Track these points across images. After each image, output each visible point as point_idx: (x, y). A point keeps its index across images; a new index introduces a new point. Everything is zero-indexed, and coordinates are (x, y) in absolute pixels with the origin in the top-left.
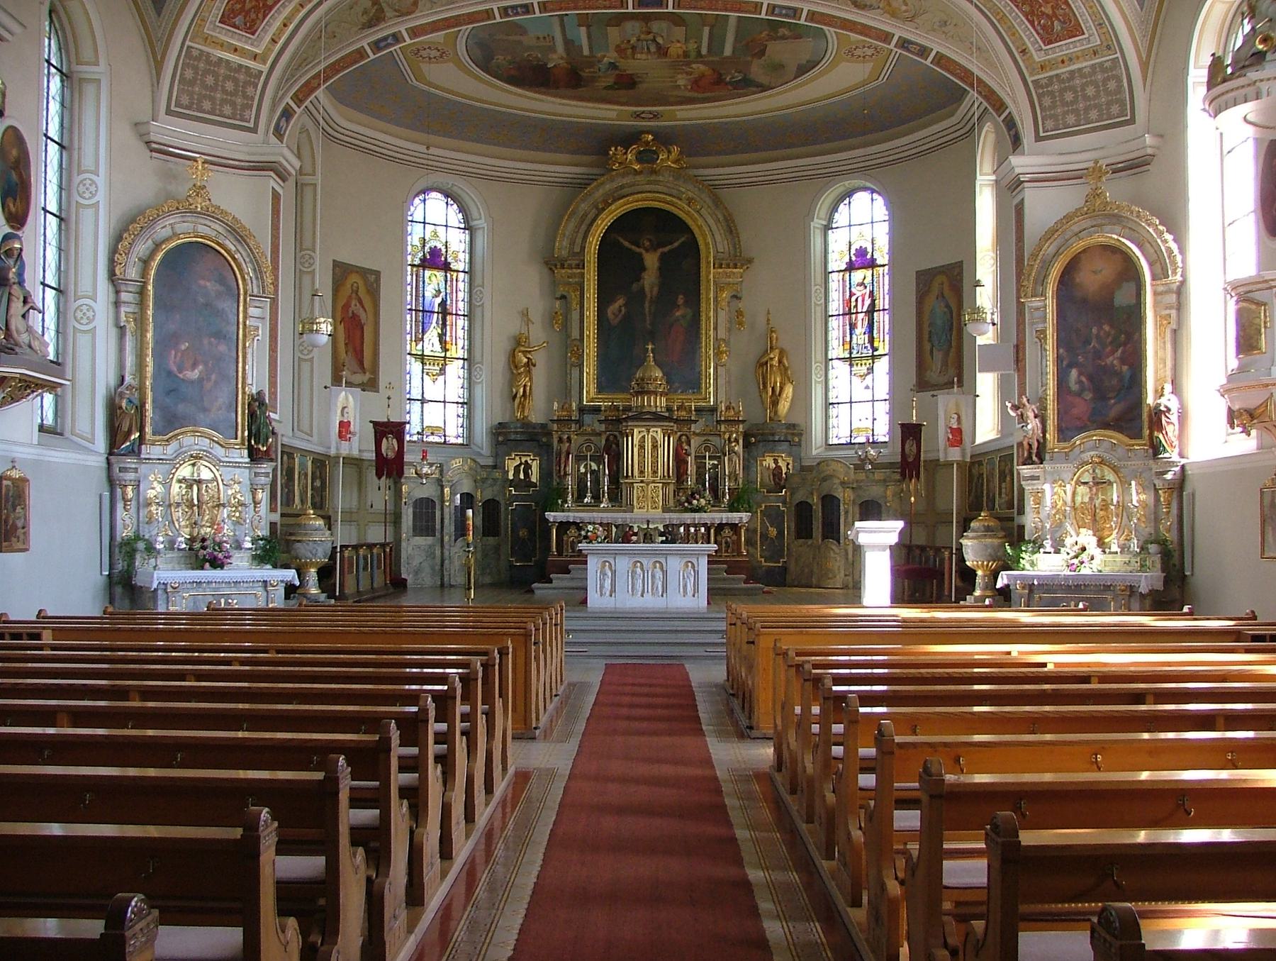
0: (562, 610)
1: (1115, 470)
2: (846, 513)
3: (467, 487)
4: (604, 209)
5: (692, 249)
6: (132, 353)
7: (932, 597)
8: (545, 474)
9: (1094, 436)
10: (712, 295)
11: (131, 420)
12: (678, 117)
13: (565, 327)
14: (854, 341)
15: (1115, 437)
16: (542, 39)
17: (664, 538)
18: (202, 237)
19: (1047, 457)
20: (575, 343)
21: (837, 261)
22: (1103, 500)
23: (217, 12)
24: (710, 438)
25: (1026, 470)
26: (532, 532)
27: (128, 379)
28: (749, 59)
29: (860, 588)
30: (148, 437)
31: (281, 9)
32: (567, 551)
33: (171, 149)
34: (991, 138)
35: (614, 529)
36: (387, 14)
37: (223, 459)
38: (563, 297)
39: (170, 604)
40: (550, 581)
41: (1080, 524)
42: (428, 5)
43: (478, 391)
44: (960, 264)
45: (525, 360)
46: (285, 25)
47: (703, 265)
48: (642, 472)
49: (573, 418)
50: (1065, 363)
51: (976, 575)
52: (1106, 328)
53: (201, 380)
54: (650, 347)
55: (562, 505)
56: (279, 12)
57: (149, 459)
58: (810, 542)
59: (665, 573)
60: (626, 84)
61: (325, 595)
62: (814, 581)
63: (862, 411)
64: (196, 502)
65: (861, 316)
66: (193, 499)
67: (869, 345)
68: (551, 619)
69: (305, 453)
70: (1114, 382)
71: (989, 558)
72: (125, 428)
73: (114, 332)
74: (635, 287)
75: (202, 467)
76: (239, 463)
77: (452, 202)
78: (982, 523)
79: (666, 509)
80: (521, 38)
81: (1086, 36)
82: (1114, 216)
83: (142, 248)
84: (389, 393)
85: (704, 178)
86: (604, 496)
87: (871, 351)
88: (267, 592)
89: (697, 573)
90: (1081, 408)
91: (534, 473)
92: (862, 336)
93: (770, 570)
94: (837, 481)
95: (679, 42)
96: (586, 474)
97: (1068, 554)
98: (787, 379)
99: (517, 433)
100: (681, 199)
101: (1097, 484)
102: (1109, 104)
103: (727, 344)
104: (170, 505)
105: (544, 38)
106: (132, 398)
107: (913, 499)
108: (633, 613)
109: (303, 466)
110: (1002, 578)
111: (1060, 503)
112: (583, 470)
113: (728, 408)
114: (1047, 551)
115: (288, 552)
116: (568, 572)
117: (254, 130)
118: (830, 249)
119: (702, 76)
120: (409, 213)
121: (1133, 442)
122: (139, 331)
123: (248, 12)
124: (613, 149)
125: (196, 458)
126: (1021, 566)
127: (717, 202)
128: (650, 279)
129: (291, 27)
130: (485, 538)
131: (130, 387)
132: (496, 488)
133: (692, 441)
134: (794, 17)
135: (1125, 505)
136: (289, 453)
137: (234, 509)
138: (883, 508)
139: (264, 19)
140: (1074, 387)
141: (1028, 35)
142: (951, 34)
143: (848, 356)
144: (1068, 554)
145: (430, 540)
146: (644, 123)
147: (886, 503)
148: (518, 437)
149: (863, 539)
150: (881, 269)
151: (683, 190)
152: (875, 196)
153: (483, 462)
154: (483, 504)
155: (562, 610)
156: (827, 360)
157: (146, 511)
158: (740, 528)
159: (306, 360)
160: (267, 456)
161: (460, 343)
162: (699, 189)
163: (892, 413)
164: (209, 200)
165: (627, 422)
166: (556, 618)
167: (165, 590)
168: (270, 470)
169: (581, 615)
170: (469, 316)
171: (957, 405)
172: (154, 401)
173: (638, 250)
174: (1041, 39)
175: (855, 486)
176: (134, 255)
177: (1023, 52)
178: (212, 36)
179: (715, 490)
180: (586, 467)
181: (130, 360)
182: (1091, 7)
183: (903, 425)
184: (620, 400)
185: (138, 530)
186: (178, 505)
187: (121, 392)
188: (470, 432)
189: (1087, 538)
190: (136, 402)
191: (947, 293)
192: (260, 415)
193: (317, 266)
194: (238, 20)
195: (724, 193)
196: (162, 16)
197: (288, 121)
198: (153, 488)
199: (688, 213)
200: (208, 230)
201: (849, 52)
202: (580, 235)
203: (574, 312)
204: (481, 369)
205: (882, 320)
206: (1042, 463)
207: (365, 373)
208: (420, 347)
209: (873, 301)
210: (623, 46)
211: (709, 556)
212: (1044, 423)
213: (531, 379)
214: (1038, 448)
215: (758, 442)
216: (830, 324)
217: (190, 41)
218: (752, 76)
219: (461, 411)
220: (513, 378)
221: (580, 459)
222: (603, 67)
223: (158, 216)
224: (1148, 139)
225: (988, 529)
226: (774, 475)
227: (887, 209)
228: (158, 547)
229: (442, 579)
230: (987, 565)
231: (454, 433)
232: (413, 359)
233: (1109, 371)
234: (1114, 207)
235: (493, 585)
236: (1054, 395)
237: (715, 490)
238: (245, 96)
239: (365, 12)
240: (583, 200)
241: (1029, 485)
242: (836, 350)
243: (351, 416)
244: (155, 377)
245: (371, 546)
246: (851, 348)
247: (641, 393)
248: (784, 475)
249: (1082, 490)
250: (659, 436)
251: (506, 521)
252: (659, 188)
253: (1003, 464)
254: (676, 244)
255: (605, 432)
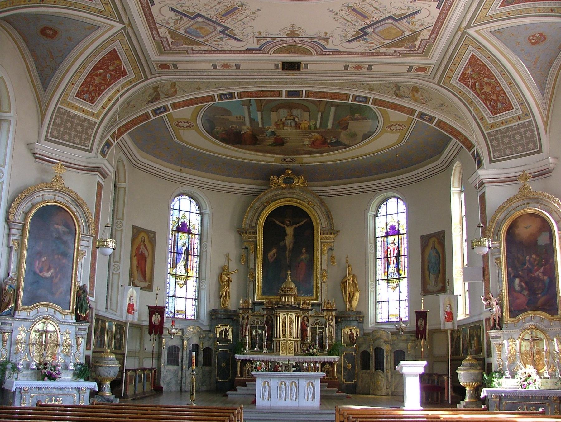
0: (242, 410)
1: (544, 332)
2: (387, 356)
3: (195, 341)
4: (267, 206)
5: (310, 226)
6: (16, 260)
7: (438, 401)
8: (235, 335)
9: (530, 314)
10: (319, 248)
11: (10, 297)
12: (304, 161)
13: (247, 262)
14: (390, 271)
15: (543, 315)
16: (239, 118)
17: (295, 369)
18: (58, 203)
19: (504, 326)
20: (251, 270)
21: (381, 232)
22: (537, 349)
23: (74, 91)
24: (318, 318)
25: (492, 333)
26: (228, 364)
27: (11, 274)
28: (340, 130)
29: (403, 396)
30: (19, 306)
31: (108, 92)
32: (245, 374)
33: (45, 158)
34: (458, 170)
35: (270, 364)
36: (161, 96)
37: (60, 320)
38: (246, 248)
39: (22, 400)
40: (236, 390)
41: (525, 362)
42: (182, 92)
43: (204, 294)
44: (443, 232)
45: (227, 278)
46: (109, 100)
47: (315, 233)
48: (284, 335)
49: (250, 307)
50: (512, 276)
51: (466, 390)
52: (534, 256)
53: (52, 277)
54: (289, 272)
55: (243, 351)
56: (107, 93)
57: (19, 318)
58: (368, 371)
59: (297, 388)
60: (280, 142)
61: (113, 396)
62: (371, 391)
63: (393, 306)
64: (44, 343)
65: (393, 259)
66: (42, 341)
67: (396, 273)
68: (235, 417)
69: (111, 320)
70: (540, 285)
71: (473, 381)
72: (7, 301)
73: (6, 249)
74: (282, 244)
75: (49, 324)
76: (70, 323)
77: (193, 201)
78: (468, 362)
79: (296, 354)
80: (229, 117)
81: (515, 110)
82: (535, 198)
83: (25, 206)
84: (157, 292)
85: (317, 192)
86: (264, 347)
87: (398, 276)
88: (80, 394)
89: (314, 388)
90: (522, 299)
91: (230, 335)
92: (394, 268)
93: (347, 386)
94: (382, 340)
95: (306, 121)
96: (256, 335)
97: (521, 379)
98: (356, 289)
99: (222, 314)
100: (304, 202)
101: (534, 340)
102: (528, 143)
103: (327, 271)
104: (29, 344)
105: (240, 117)
106: (12, 285)
107: (422, 349)
108: (280, 410)
109: (110, 327)
110: (484, 392)
111: (513, 351)
112: (254, 333)
113: (328, 303)
114: (507, 377)
115: (95, 372)
116: (246, 386)
117: (90, 151)
118: (378, 225)
119: (317, 139)
120: (172, 205)
121: (553, 317)
122: (19, 250)
123: (91, 92)
124: (272, 177)
125: (46, 319)
126: (493, 385)
127: (322, 203)
128: (289, 240)
129: (113, 101)
130: (204, 367)
131: (12, 279)
132: (210, 342)
133: (310, 320)
134: (365, 102)
135: (551, 351)
136: (100, 319)
137: (65, 348)
138: (406, 354)
139: (99, 96)
140: (517, 288)
141: (485, 111)
142: (445, 110)
143: (387, 278)
144: (521, 379)
145: (176, 367)
146: (287, 164)
147: (407, 351)
148: (222, 316)
149: (405, 371)
150: (403, 235)
151: (305, 197)
152: (399, 200)
153: (204, 328)
154: (204, 350)
155: (242, 410)
156: (376, 280)
157: (15, 347)
158: (334, 364)
159: (116, 274)
160: (85, 320)
161: (195, 269)
162: (313, 197)
163: (409, 307)
164: (63, 184)
165: (277, 309)
166: (238, 416)
167: (20, 392)
168: (87, 327)
169: (252, 410)
170: (200, 256)
171: (450, 301)
172: (25, 287)
173: (282, 225)
174: (491, 112)
175: (391, 343)
176: (20, 210)
177: (482, 119)
178: (71, 103)
179: (321, 344)
180: (256, 332)
181: (13, 265)
182: (517, 95)
183: (416, 312)
184: (273, 299)
185: (9, 358)
186: (33, 344)
187: (6, 281)
188: (198, 313)
189: (531, 370)
190: (15, 288)
191: (437, 246)
192: (83, 297)
193: (124, 228)
194: (86, 96)
195: (325, 199)
196: (47, 91)
197: (108, 148)
198: (20, 335)
199: (308, 208)
200: (62, 200)
201: (389, 127)
202: (255, 218)
203: (251, 255)
204: (205, 282)
205: (404, 261)
206: (501, 329)
207: (146, 282)
208: (174, 270)
209: (399, 251)
210: (279, 123)
211: (321, 379)
212: (501, 307)
213: (229, 288)
214: (499, 321)
215: (342, 320)
216: (377, 263)
217: (60, 104)
218: (340, 140)
219: (194, 303)
220: (221, 287)
221: (253, 328)
222: (268, 134)
223: (35, 190)
224: (551, 160)
225: (472, 365)
226: (350, 337)
227: (405, 206)
228: (19, 367)
229: (181, 388)
230: (472, 385)
231: (190, 314)
232: (171, 276)
233: (538, 279)
234: (534, 194)
235: (209, 391)
236: (506, 292)
237: (321, 344)
238: (86, 134)
239: (150, 95)
240: (257, 201)
241: (494, 341)
242: (381, 275)
243: (134, 301)
244: (26, 274)
245: (143, 370)
246: (388, 274)
247: (284, 295)
248: (355, 338)
249: (524, 343)
250: (293, 317)
251: (215, 359)
252: (295, 196)
253: (472, 331)
254: (302, 223)
255: (266, 314)
